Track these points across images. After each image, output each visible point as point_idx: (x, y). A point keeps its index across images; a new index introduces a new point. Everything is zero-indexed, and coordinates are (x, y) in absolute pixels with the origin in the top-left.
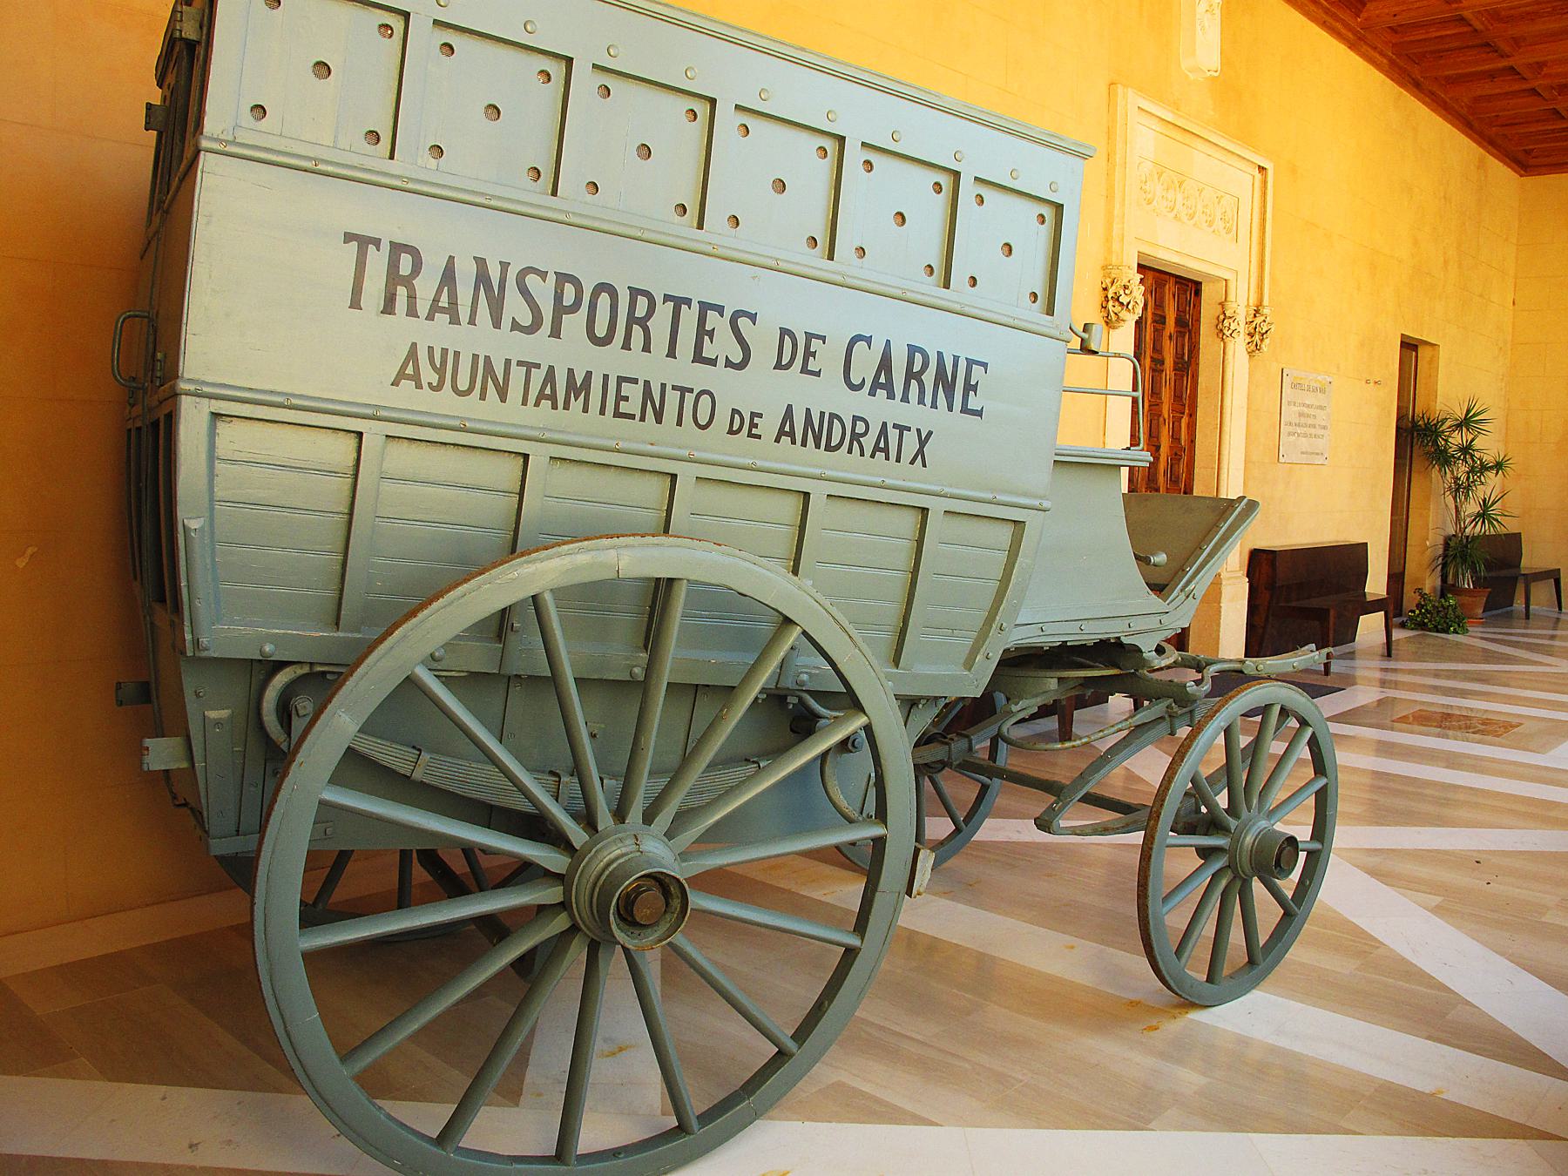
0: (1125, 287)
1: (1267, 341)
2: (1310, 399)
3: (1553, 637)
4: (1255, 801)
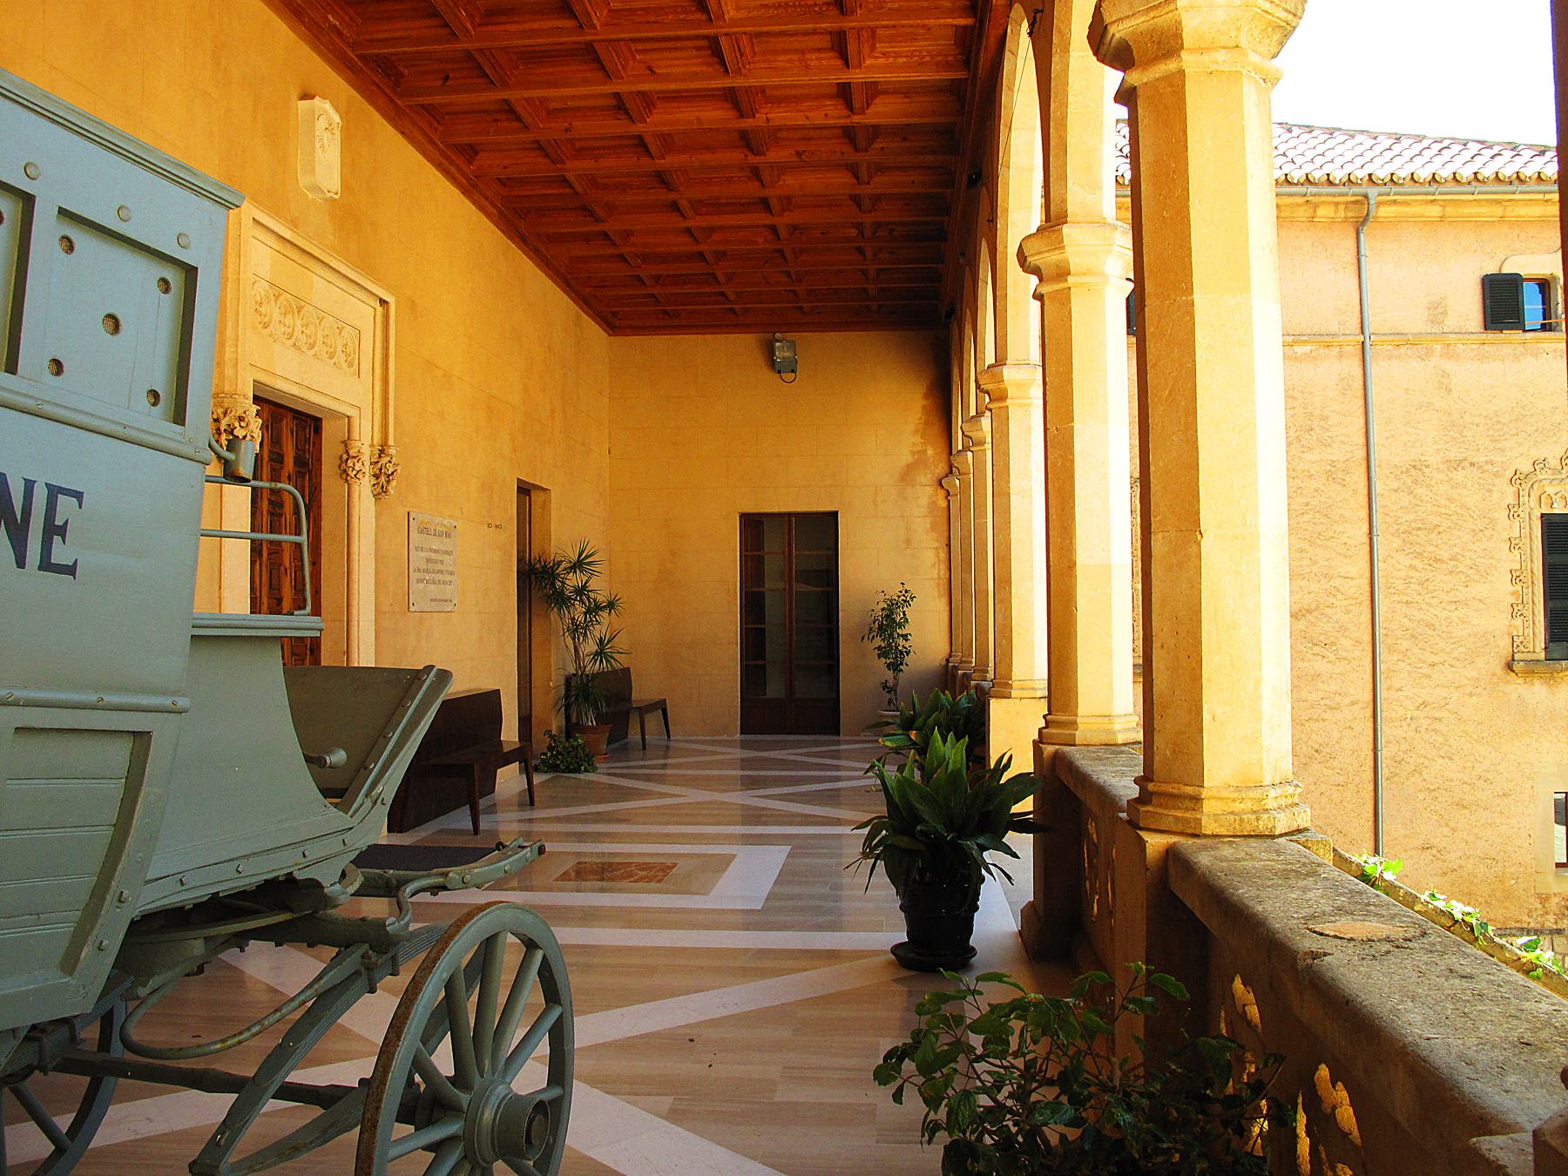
0: (241, 419)
1: (394, 483)
2: (435, 544)
3: (665, 766)
4: (487, 1063)
